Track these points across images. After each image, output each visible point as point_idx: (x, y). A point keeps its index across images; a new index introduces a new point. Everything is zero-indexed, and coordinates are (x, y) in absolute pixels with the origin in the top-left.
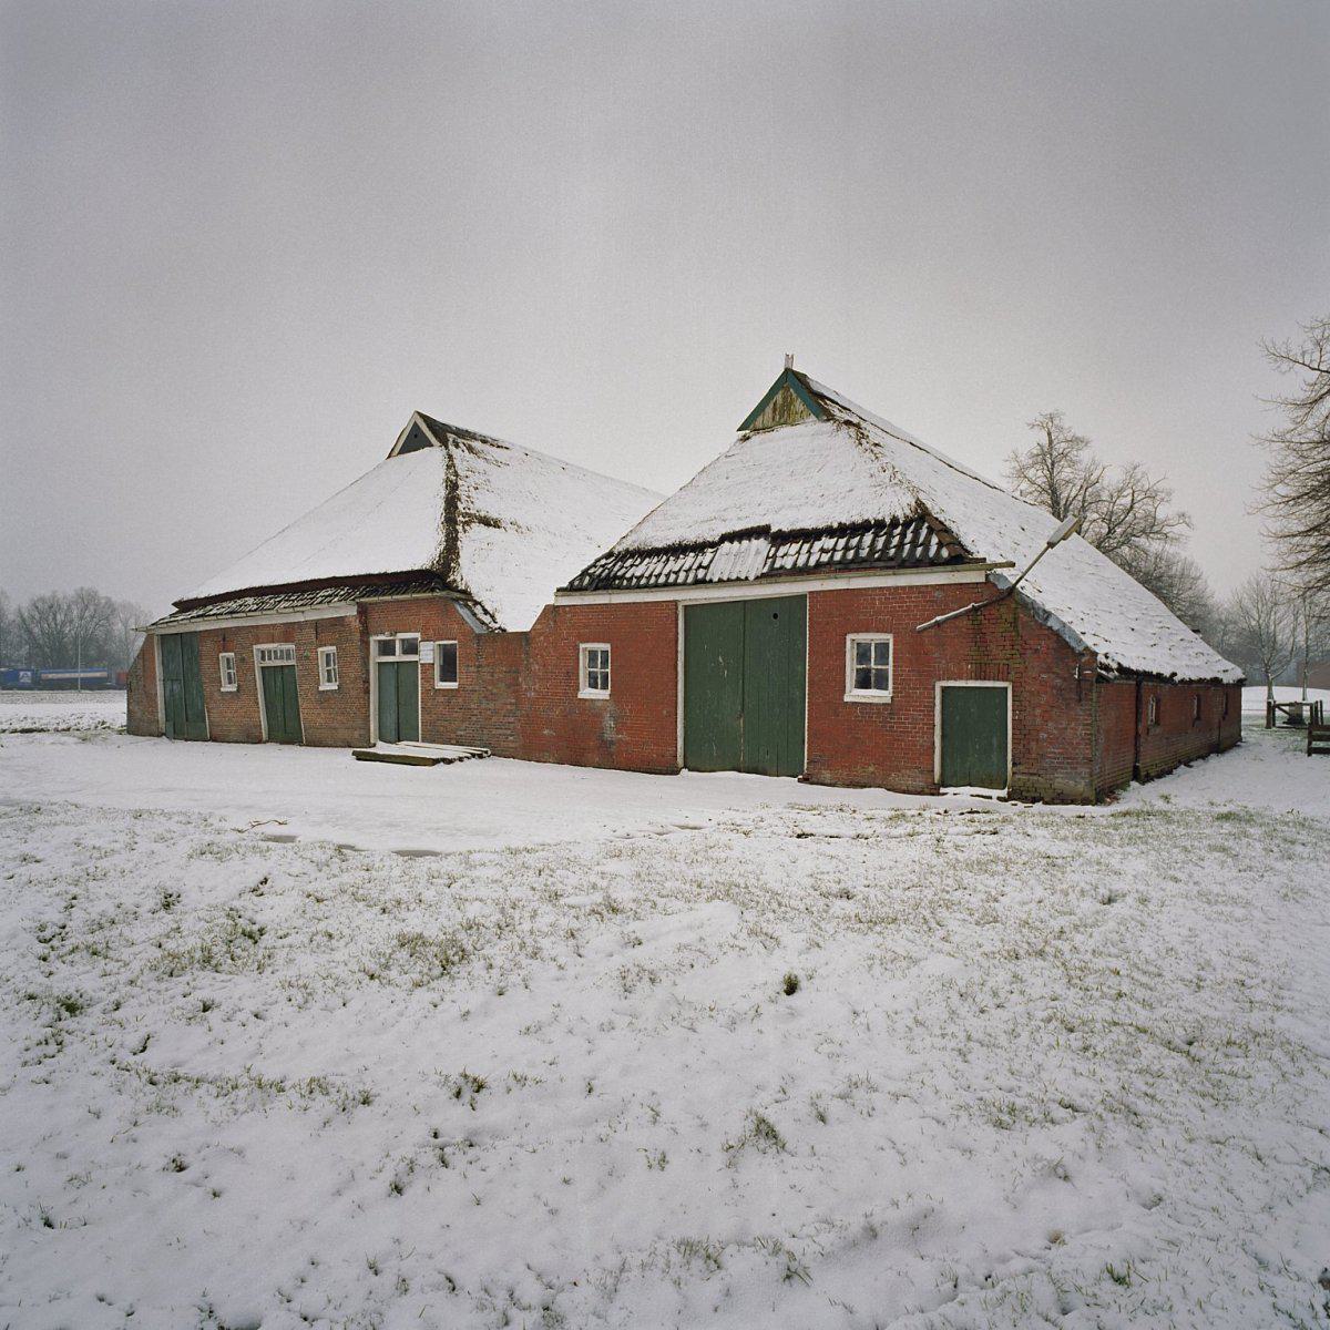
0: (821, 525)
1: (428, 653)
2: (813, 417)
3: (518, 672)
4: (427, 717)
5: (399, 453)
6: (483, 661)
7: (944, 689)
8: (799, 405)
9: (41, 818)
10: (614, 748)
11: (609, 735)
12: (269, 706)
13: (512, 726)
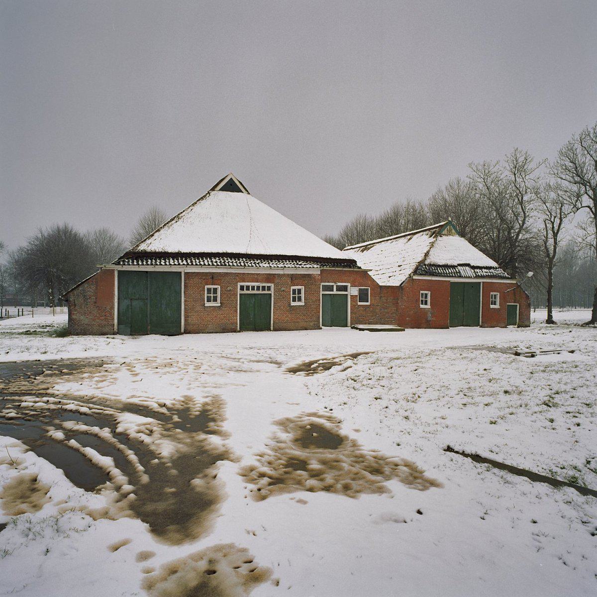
0: (482, 266)
1: (354, 291)
2: (457, 235)
3: (398, 299)
4: (126, 302)
5: (221, 190)
6: (382, 295)
7: (517, 305)
8: (453, 231)
9: (341, 478)
10: (430, 323)
11: (429, 319)
12: (440, 327)
13: (394, 317)
